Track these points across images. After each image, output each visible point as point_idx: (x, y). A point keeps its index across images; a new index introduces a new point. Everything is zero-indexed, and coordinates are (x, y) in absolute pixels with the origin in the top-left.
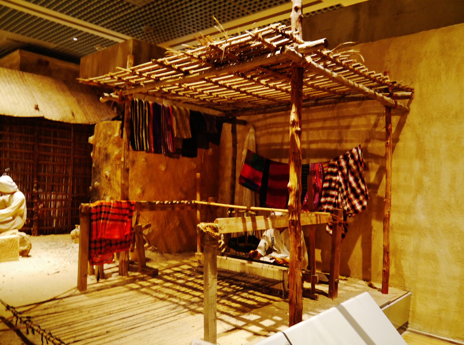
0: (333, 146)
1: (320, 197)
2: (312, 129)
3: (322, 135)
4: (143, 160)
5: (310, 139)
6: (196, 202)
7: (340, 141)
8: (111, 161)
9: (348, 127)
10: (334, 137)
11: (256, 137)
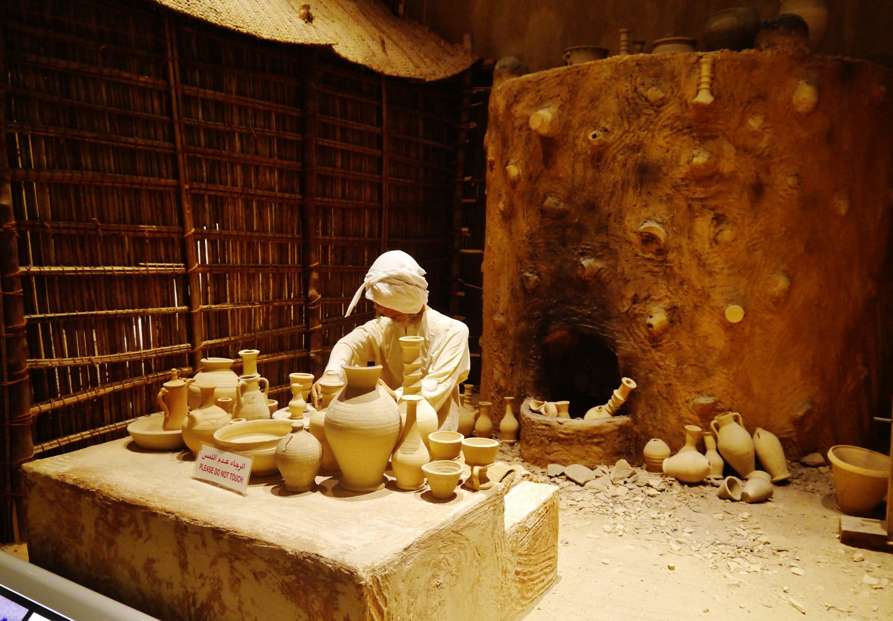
4: (791, 181)
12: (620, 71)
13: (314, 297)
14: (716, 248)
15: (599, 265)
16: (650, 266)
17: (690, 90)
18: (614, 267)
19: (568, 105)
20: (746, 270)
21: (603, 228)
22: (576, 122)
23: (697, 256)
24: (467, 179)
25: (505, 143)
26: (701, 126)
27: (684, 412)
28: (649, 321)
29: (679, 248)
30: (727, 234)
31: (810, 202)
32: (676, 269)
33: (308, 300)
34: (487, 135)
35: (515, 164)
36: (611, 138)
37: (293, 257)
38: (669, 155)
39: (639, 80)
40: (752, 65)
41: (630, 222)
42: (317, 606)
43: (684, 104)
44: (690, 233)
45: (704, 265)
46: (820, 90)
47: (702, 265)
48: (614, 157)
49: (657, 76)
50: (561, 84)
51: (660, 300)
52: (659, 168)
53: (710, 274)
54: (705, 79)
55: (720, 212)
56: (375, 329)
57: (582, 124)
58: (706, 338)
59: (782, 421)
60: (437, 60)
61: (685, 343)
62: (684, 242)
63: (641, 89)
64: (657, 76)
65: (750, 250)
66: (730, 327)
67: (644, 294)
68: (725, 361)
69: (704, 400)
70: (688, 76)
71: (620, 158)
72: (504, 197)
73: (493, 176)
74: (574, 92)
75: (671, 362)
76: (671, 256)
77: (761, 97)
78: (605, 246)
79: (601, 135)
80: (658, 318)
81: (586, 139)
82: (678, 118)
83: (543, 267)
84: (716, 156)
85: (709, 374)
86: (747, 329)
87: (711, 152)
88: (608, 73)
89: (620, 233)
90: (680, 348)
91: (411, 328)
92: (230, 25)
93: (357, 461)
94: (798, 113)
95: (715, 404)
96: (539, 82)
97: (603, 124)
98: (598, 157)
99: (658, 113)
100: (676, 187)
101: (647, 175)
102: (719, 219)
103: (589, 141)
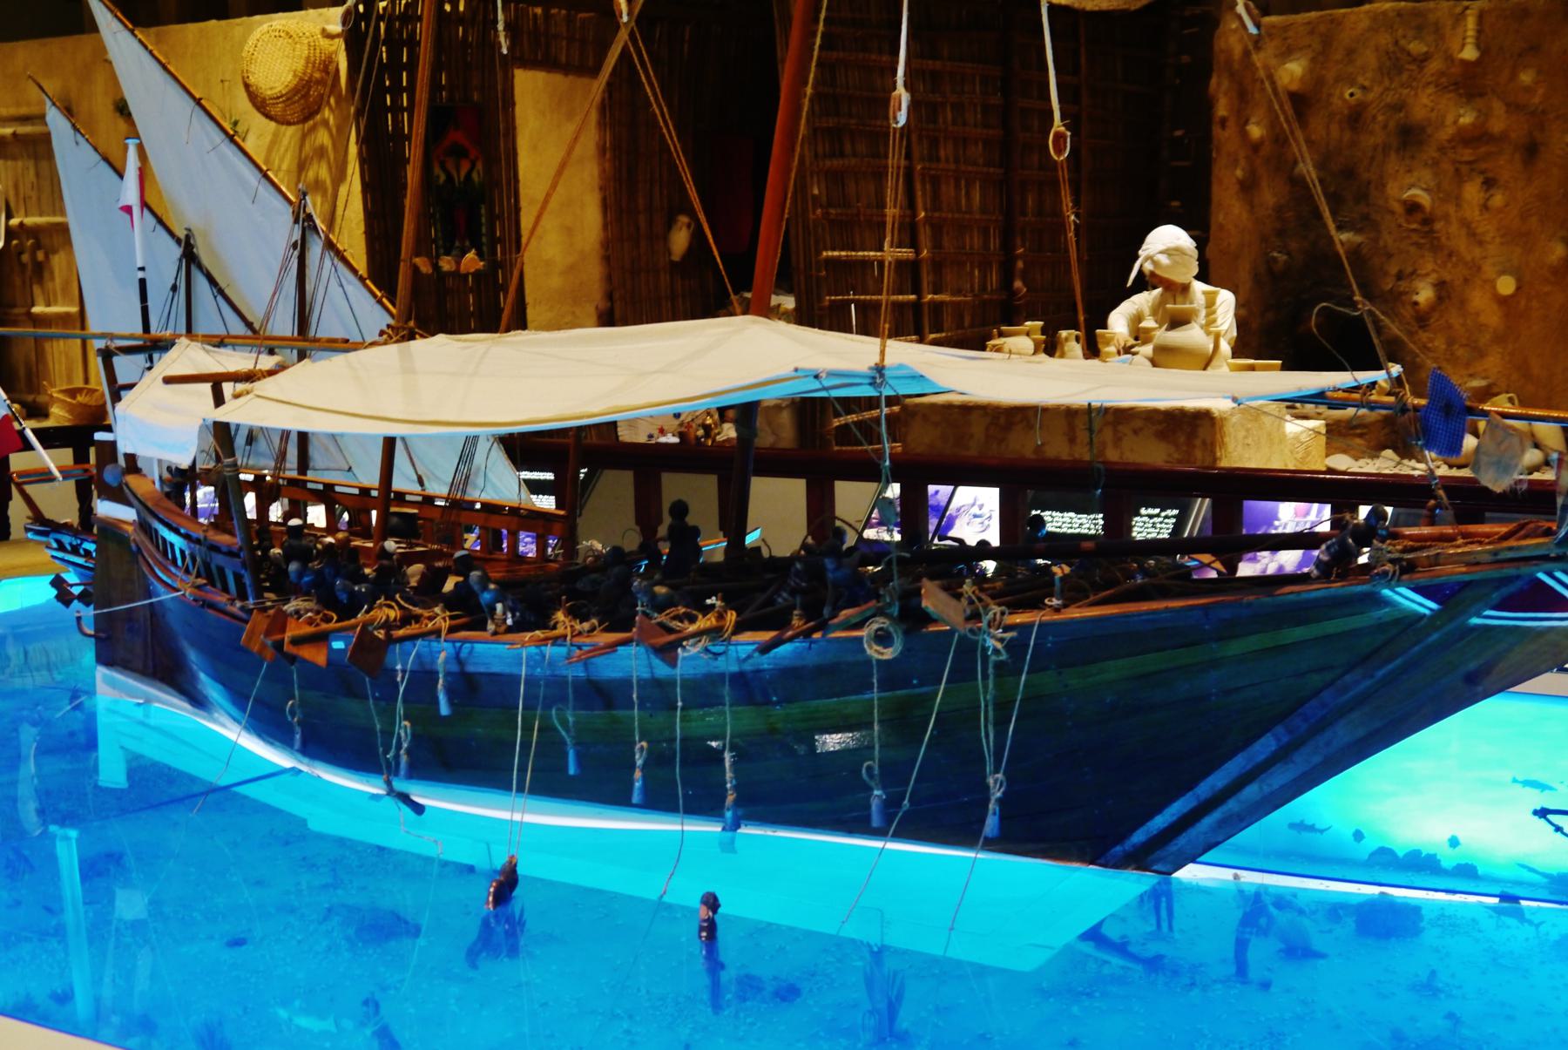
8: (1431, 152)
13: (1019, 290)
14: (1487, 216)
15: (1358, 239)
16: (1415, 237)
17: (1455, 46)
18: (1376, 240)
19: (1319, 59)
21: (1362, 197)
22: (1330, 75)
23: (1466, 224)
24: (1178, 133)
25: (1243, 97)
26: (1467, 83)
28: (1415, 298)
29: (1446, 217)
30: (1498, 200)
32: (1443, 239)
33: (1013, 293)
34: (1214, 81)
35: (1258, 124)
36: (1371, 96)
37: (994, 243)
38: (1434, 115)
39: (1400, 32)
41: (1392, 189)
42: (1182, 439)
43: (1449, 58)
44: (1458, 201)
45: (1474, 235)
47: (1472, 234)
48: (1374, 117)
49: (1420, 28)
50: (1312, 32)
51: (1427, 275)
52: (1422, 129)
53: (1481, 243)
54: (1470, 33)
55: (1490, 175)
56: (1142, 301)
57: (1338, 80)
58: (1478, 314)
61: (1455, 320)
62: (1452, 209)
63: (1402, 42)
64: (1420, 28)
65: (1524, 216)
66: (1503, 301)
67: (1410, 270)
68: (1499, 339)
69: (1476, 383)
70: (1454, 28)
71: (1380, 118)
72: (1243, 162)
73: (1225, 137)
74: (1327, 42)
75: (1440, 343)
76: (1438, 226)
78: (1366, 217)
79: (1359, 94)
80: (1424, 294)
81: (1341, 97)
82: (1442, 74)
83: (1294, 245)
84: (1484, 115)
85: (1481, 354)
86: (1523, 303)
87: (1479, 111)
88: (1365, 23)
89: (1381, 202)
90: (1450, 327)
91: (1179, 299)
94: (1384, 186)
95: (1489, 387)
96: (1286, 28)
97: (1361, 80)
98: (1356, 118)
99: (1421, 68)
100: (1441, 149)
101: (1410, 137)
102: (1489, 184)
103: (1345, 101)
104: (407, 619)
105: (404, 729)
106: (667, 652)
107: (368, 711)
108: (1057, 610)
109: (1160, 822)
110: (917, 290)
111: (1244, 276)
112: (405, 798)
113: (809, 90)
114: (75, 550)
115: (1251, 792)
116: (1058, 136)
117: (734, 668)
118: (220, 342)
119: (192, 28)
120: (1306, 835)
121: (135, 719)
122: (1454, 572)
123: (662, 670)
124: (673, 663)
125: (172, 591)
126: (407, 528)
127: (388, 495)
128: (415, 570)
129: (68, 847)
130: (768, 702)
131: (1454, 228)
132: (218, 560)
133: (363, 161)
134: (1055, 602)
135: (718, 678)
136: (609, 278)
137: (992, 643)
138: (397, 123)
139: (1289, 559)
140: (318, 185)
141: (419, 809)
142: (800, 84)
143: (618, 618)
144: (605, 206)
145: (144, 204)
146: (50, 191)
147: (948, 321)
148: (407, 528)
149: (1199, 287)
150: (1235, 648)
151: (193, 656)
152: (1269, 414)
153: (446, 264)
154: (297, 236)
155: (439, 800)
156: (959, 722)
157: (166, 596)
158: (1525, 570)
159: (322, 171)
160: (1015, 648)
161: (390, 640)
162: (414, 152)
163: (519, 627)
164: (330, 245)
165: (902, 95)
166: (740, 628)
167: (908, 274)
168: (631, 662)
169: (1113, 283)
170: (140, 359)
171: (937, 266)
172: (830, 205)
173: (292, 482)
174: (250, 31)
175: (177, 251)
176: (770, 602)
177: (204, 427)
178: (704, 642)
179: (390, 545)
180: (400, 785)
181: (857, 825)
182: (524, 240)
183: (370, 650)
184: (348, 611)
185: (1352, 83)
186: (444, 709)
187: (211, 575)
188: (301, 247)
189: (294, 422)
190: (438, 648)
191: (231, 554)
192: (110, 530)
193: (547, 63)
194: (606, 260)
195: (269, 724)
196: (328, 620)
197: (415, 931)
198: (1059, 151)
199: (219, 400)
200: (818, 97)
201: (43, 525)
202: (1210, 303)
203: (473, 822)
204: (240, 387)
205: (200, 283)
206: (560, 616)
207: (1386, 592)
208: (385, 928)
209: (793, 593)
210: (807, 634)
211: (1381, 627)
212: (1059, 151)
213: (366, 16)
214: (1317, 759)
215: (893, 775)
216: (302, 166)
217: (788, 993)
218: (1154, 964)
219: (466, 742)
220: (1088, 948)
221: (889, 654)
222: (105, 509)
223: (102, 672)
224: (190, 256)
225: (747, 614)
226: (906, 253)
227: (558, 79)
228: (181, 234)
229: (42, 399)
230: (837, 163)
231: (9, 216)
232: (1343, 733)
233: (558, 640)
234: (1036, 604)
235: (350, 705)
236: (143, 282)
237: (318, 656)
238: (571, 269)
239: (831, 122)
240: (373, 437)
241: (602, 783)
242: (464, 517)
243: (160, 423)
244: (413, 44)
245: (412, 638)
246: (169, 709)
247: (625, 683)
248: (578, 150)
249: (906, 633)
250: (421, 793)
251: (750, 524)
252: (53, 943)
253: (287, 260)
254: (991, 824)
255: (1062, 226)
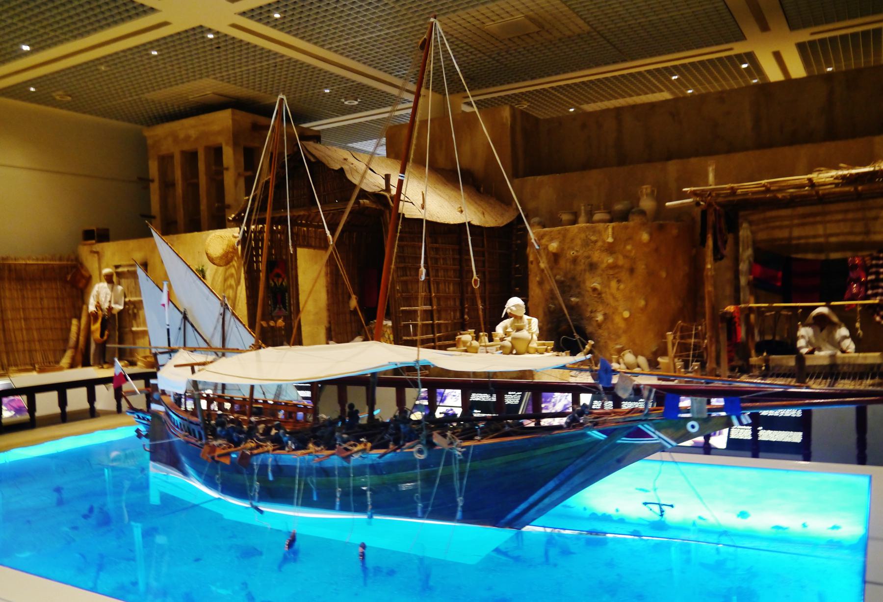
0: (858, 239)
1: (867, 290)
2: (829, 222)
3: (844, 228)
4: (643, 267)
5: (829, 231)
6: (751, 305)
7: (867, 233)
8: (599, 272)
9: (876, 218)
10: (859, 227)
11: (753, 232)
12: (581, 230)
17: (605, 237)
19: (562, 242)
20: (629, 299)
21: (578, 286)
22: (566, 247)
26: (610, 249)
27: (612, 352)
30: (622, 286)
31: (651, 274)
37: (458, 303)
40: (626, 228)
43: (604, 242)
44: (609, 287)
46: (651, 235)
47: (614, 298)
53: (617, 301)
57: (569, 248)
59: (648, 353)
60: (502, 215)
61: (611, 327)
65: (631, 292)
66: (626, 320)
68: (625, 332)
69: (618, 347)
73: (532, 267)
74: (564, 236)
75: (606, 334)
77: (630, 238)
78: (579, 293)
80: (600, 318)
84: (616, 259)
85: (619, 337)
88: (576, 230)
92: (442, 221)
93: (521, 346)
96: (551, 232)
98: (575, 261)
100: (603, 271)
102: (619, 281)
104: (258, 447)
105: (257, 485)
106: (347, 458)
107: (243, 478)
108: (479, 441)
109: (517, 511)
110: (432, 319)
111: (541, 312)
112: (257, 509)
113: (393, 266)
114: (144, 419)
115: (547, 501)
116: (476, 280)
117: (370, 462)
118: (193, 350)
119: (189, 235)
120: (568, 509)
121: (163, 479)
122: (612, 426)
123: (345, 464)
124: (349, 462)
125: (178, 437)
126: (259, 412)
127: (252, 400)
128: (261, 427)
129: (137, 530)
130: (382, 474)
131: (609, 296)
132: (193, 426)
133: (246, 279)
134: (478, 438)
135: (365, 466)
136: (329, 316)
137: (458, 452)
138: (258, 266)
139: (557, 421)
140: (231, 286)
141: (261, 512)
142: (391, 264)
143: (330, 446)
144: (328, 292)
145: (169, 300)
146: (137, 291)
147: (443, 329)
148: (259, 412)
149: (526, 317)
150: (539, 452)
151: (183, 459)
152: (546, 364)
153: (272, 323)
154: (222, 311)
155: (268, 508)
156: (447, 479)
157: (175, 439)
158: (634, 424)
159: (232, 282)
160: (465, 454)
161: (252, 455)
162: (262, 275)
163: (297, 449)
164: (233, 314)
165: (423, 270)
166: (372, 448)
167: (429, 314)
168: (335, 461)
169: (495, 315)
170: (167, 356)
171: (439, 311)
172: (403, 292)
173: (219, 396)
174: (208, 235)
175: (181, 316)
176: (383, 438)
177: (188, 381)
178: (360, 454)
179: (253, 419)
180: (255, 504)
181: (413, 514)
182: (301, 306)
183: (245, 459)
184: (237, 444)
185: (573, 249)
186: (271, 478)
187: (190, 432)
188: (223, 315)
189: (220, 380)
190: (269, 456)
191: (197, 425)
192: (155, 414)
193: (308, 246)
194: (329, 310)
195: (210, 482)
196: (230, 447)
197: (261, 554)
198: (476, 285)
199: (193, 372)
200: (398, 257)
201: (133, 410)
202: (530, 323)
203: (282, 516)
204: (201, 367)
205: (188, 326)
206: (311, 445)
207: (589, 433)
208: (249, 553)
209: (390, 435)
210: (395, 450)
211: (588, 444)
212: (476, 285)
213: (247, 232)
214: (568, 489)
215: (425, 497)
216: (225, 280)
217: (391, 573)
218: (517, 559)
219: (278, 488)
220: (494, 554)
221: (422, 457)
222: (154, 407)
223: (152, 464)
224: (185, 318)
225: (375, 443)
226: (428, 307)
227: (311, 251)
228: (182, 310)
229: (135, 359)
230: (405, 278)
231: (125, 297)
232: (577, 480)
233: (309, 454)
234: (471, 438)
235: (239, 477)
236: (168, 330)
237: (227, 461)
238: (317, 313)
239: (402, 265)
240: (246, 385)
241: (326, 502)
242: (279, 407)
243: (173, 379)
244: (262, 240)
245: (259, 454)
246: (175, 476)
247: (333, 468)
248: (318, 284)
249: (429, 449)
250: (263, 506)
251: (376, 407)
252: (133, 563)
253: (218, 319)
254: (459, 515)
255: (478, 310)
